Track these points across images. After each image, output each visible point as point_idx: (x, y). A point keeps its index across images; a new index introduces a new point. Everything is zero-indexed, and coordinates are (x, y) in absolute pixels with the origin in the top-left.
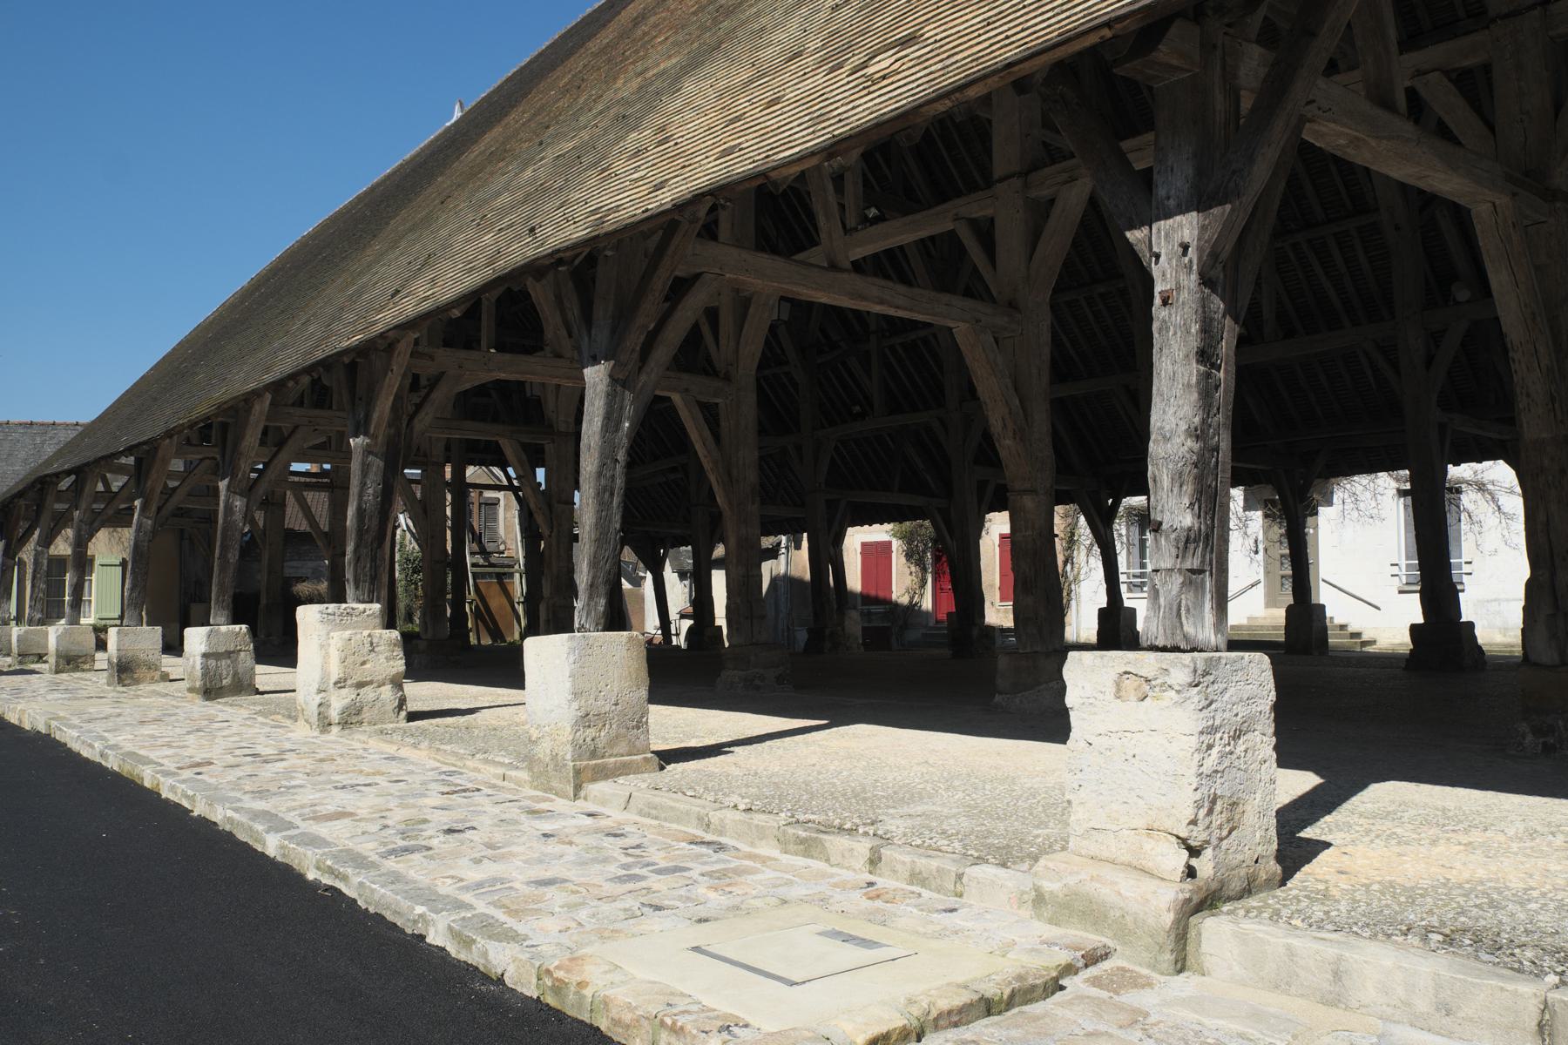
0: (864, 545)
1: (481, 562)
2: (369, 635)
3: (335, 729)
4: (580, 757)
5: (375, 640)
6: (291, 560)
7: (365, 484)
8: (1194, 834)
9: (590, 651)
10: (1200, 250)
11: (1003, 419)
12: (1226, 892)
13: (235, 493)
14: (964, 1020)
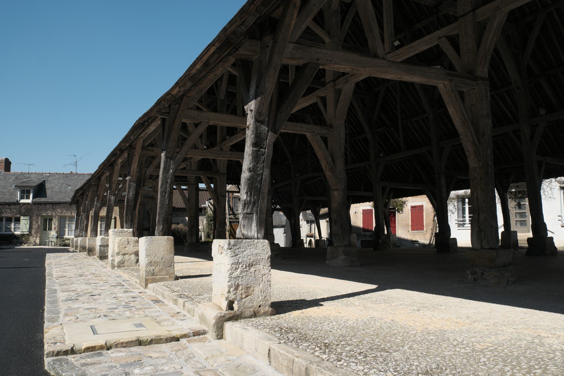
0: (363, 210)
1: (233, 217)
2: (127, 239)
3: (116, 268)
4: (148, 275)
5: (129, 240)
6: (175, 217)
7: (129, 191)
8: (230, 296)
9: (153, 242)
10: (255, 111)
11: (325, 165)
12: (243, 315)
13: (112, 195)
14: (128, 346)
